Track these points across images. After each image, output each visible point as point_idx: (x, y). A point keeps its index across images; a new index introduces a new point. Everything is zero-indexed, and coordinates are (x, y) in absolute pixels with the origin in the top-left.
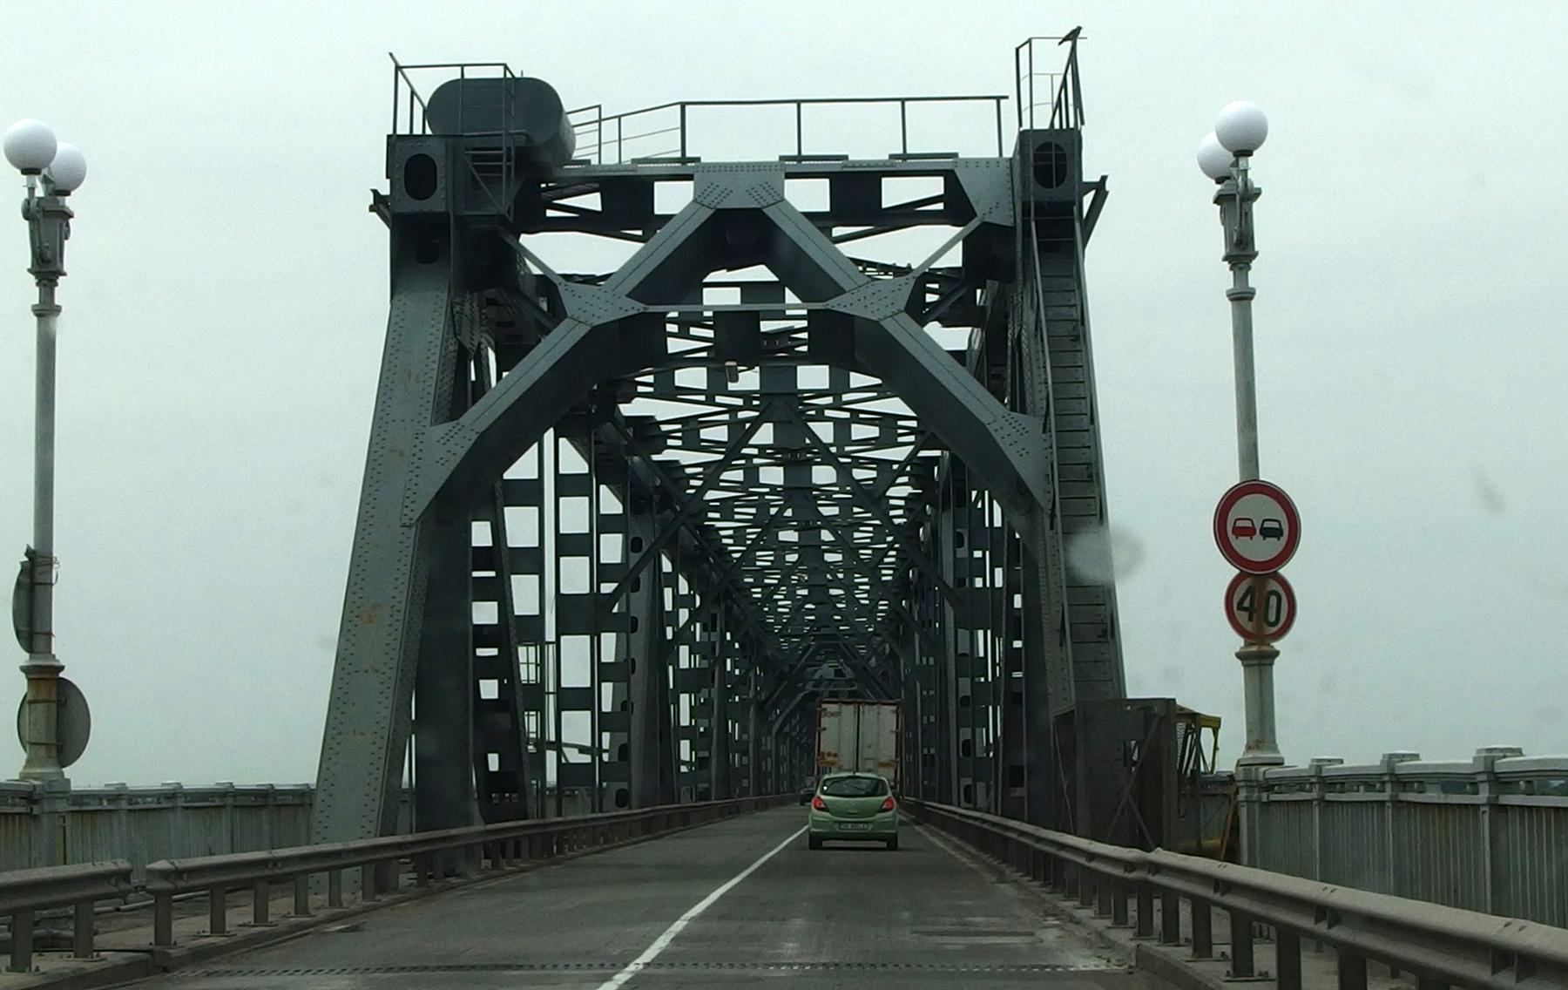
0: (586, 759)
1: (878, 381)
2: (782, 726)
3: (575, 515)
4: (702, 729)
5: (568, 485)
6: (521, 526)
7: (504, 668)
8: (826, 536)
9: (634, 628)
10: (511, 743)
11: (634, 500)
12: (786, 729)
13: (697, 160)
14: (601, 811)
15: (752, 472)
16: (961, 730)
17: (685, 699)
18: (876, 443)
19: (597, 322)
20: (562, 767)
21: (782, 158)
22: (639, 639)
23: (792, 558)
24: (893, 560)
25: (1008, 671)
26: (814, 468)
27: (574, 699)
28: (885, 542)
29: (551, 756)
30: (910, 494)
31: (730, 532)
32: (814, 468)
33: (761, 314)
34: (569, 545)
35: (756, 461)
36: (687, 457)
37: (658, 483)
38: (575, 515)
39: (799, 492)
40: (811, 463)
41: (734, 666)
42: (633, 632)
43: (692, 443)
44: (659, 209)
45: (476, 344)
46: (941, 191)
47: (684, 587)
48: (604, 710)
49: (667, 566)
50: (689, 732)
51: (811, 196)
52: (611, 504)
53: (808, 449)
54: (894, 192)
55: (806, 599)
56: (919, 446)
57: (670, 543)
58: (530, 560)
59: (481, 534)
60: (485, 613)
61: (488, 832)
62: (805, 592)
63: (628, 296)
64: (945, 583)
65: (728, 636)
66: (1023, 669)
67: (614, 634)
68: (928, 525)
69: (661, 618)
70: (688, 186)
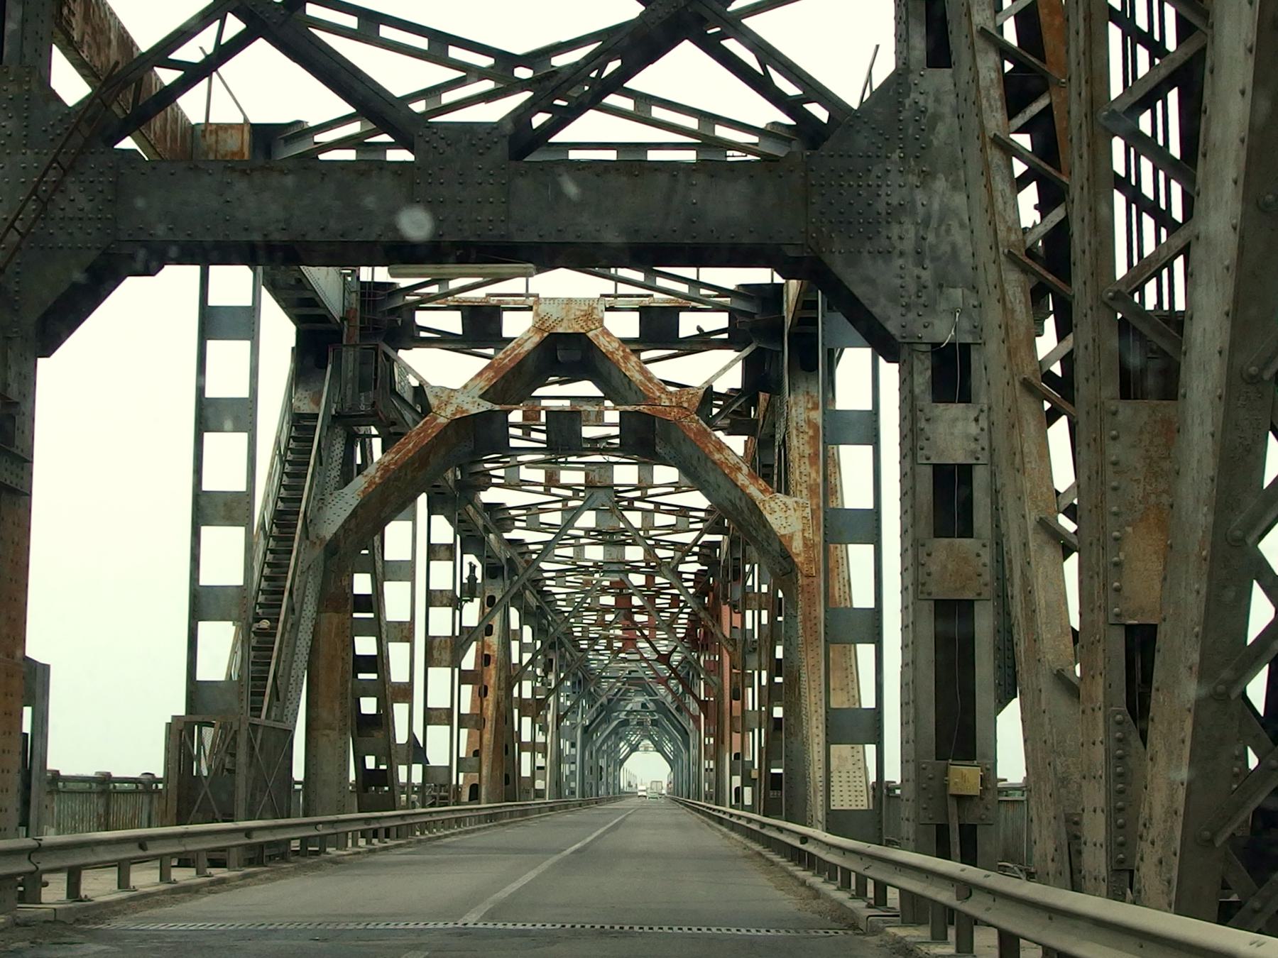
23: (609, 617)
44: (506, 333)
68: (711, 594)
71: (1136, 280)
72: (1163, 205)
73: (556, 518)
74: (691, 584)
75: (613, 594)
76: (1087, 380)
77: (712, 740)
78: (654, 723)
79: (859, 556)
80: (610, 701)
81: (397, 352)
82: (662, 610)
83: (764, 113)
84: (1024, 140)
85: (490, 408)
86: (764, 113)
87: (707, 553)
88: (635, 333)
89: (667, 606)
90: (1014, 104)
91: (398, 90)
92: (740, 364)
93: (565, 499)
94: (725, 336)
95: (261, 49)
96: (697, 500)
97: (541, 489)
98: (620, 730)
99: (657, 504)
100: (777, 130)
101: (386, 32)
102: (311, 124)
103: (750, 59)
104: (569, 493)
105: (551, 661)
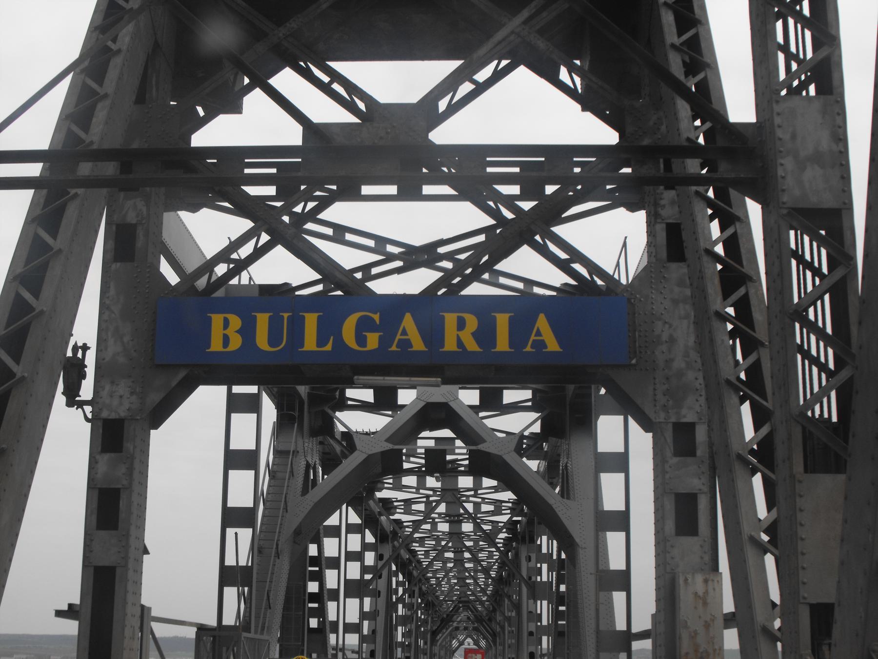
2: (442, 642)
3: (354, 542)
6: (331, 547)
7: (321, 613)
8: (467, 555)
11: (382, 537)
15: (434, 525)
16: (529, 647)
19: (370, 453)
22: (382, 601)
23: (450, 565)
27: (350, 628)
31: (423, 552)
34: (352, 556)
35: (436, 520)
37: (408, 557)
38: (354, 542)
39: (456, 535)
40: (464, 551)
43: (408, 511)
44: (400, 402)
47: (401, 578)
49: (394, 568)
50: (402, 644)
52: (370, 538)
53: (461, 515)
58: (334, 563)
59: (313, 550)
60: (313, 587)
66: (566, 619)
68: (513, 551)
69: (391, 591)
71: (809, 405)
72: (806, 347)
73: (421, 507)
74: (501, 545)
75: (453, 552)
76: (784, 462)
77: (513, 641)
78: (475, 629)
79: (614, 540)
80: (448, 615)
81: (335, 413)
82: (483, 561)
83: (558, 278)
84: (731, 311)
85: (391, 448)
86: (558, 278)
87: (511, 526)
88: (477, 403)
89: (486, 558)
90: (726, 295)
91: (348, 265)
92: (539, 422)
93: (428, 497)
94: (530, 404)
95: (279, 251)
96: (508, 496)
97: (414, 490)
98: (453, 633)
99: (483, 499)
100: (567, 289)
101: (349, 237)
102: (294, 285)
103: (553, 248)
104: (431, 493)
105: (414, 591)
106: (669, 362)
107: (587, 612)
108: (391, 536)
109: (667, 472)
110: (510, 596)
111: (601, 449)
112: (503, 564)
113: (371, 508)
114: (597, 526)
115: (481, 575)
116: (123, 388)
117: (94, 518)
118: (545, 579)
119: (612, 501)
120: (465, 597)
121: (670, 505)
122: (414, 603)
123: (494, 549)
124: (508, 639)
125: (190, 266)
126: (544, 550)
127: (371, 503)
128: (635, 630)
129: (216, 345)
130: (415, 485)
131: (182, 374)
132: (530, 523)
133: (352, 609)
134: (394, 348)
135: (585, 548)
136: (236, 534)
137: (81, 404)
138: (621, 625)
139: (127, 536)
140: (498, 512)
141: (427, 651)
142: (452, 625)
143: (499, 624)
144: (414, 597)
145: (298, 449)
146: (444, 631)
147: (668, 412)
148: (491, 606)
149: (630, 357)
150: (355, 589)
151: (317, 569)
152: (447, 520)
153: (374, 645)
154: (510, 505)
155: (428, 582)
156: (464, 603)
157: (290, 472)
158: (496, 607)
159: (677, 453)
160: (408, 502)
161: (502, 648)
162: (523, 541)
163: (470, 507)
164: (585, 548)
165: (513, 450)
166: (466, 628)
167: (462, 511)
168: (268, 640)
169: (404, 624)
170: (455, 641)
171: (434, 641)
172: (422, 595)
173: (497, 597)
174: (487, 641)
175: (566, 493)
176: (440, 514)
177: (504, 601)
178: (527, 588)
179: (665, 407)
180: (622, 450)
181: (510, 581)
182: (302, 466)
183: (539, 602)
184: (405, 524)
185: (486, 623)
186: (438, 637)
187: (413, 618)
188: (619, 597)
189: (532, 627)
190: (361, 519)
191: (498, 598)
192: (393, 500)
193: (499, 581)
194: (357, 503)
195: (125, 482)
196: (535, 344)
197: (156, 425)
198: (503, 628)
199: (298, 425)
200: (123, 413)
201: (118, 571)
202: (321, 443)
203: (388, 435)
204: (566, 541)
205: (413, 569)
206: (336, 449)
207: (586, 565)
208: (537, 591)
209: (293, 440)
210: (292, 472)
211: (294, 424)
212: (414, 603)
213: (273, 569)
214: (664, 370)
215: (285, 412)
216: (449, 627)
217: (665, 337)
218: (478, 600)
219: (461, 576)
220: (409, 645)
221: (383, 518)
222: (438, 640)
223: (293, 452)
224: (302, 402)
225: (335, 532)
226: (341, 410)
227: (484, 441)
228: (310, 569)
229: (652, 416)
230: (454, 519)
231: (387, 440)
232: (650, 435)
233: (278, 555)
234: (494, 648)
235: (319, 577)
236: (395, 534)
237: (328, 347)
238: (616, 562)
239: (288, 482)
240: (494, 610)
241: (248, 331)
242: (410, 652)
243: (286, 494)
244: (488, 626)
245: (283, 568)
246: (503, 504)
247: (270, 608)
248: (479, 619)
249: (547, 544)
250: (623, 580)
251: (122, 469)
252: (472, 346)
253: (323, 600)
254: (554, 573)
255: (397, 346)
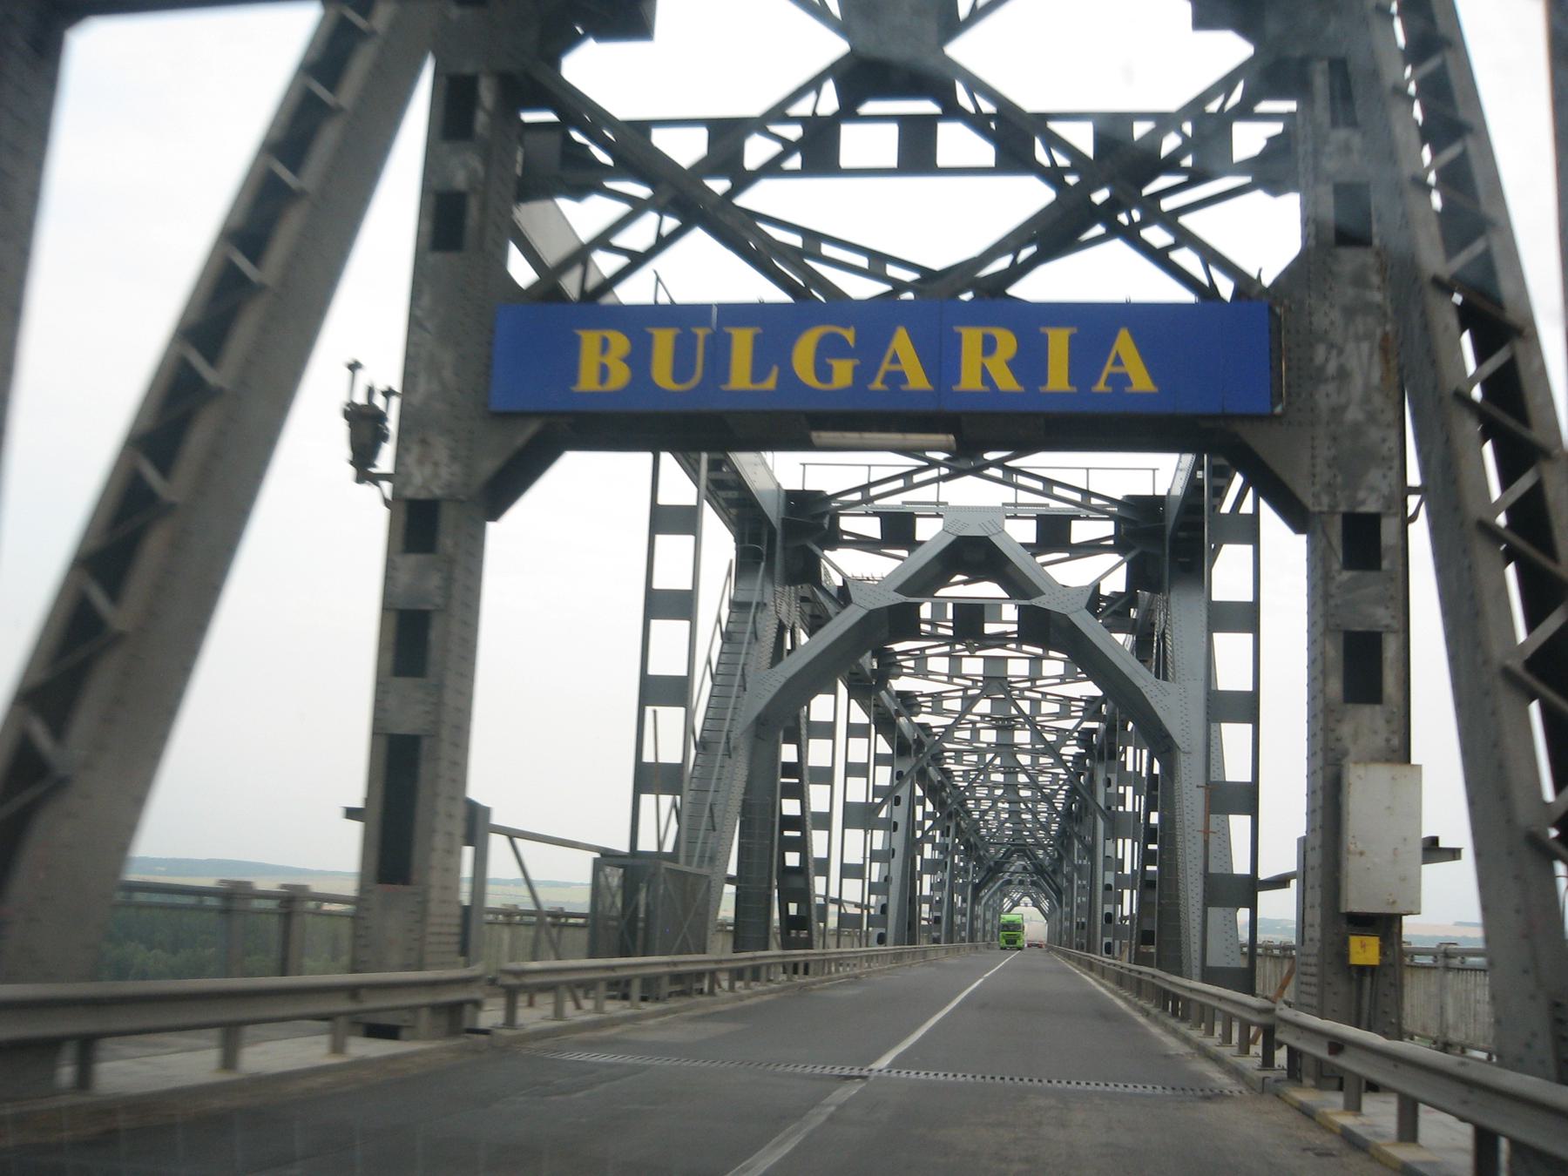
0: (858, 911)
1: (1066, 656)
2: (988, 900)
3: (859, 750)
4: (937, 899)
5: (854, 731)
6: (819, 753)
7: (802, 846)
8: (1022, 778)
9: (895, 828)
10: (804, 895)
11: (902, 747)
12: (991, 902)
13: (946, 503)
14: (867, 946)
15: (975, 732)
16: (1105, 906)
17: (927, 879)
18: (1058, 716)
19: (872, 607)
20: (842, 918)
21: (1004, 504)
22: (899, 839)
23: (999, 792)
24: (1063, 797)
25: (1143, 864)
26: (1016, 732)
27: (848, 871)
28: (1058, 784)
29: (833, 909)
30: (1077, 753)
31: (961, 773)
32: (1016, 732)
33: (987, 611)
34: (853, 770)
35: (978, 725)
36: (935, 721)
37: (939, 779)
38: (859, 750)
39: (1006, 748)
40: (1017, 773)
41: (961, 860)
42: (894, 831)
43: (938, 711)
44: (918, 538)
45: (791, 622)
46: (1112, 532)
47: (929, 807)
48: (873, 880)
49: (919, 792)
50: (929, 900)
51: (1024, 532)
52: (884, 747)
53: (1013, 718)
54: (1081, 532)
55: (1006, 820)
56: (1083, 720)
57: (922, 776)
58: (825, 776)
59: (788, 753)
60: (791, 807)
61: (784, 956)
62: (1007, 816)
63: (895, 591)
64: (1097, 804)
65: (957, 840)
66: (1158, 863)
67: (882, 832)
68: (1087, 774)
69: (912, 824)
70: (940, 521)
78: (1033, 883)
79: (1234, 736)
80: (996, 863)
85: (904, 601)
94: (1111, 542)
99: (1044, 694)
102: (829, 493)
104: (969, 683)
106: (1338, 411)
107: (1189, 848)
108: (914, 747)
109: (1332, 596)
110: (1081, 837)
111: (1215, 598)
112: (1070, 794)
113: (883, 703)
114: (1208, 713)
115: (1042, 807)
116: (441, 448)
117: (389, 657)
118: (1129, 808)
119: (1232, 675)
120: (1019, 839)
121: (1334, 652)
122: (947, 845)
123: (1061, 771)
124: (1078, 896)
125: (551, 256)
126: (1130, 768)
127: (883, 693)
128: (1263, 875)
129: (588, 381)
130: (947, 671)
131: (533, 427)
132: (1111, 730)
133: (854, 847)
134: (878, 385)
135: (1189, 753)
136: (655, 712)
137: (375, 479)
138: (1241, 866)
139: (440, 687)
140: (1064, 714)
141: (966, 911)
142: (1002, 877)
143: (1066, 876)
144: (948, 836)
145: (766, 601)
146: (991, 885)
147: (1335, 495)
148: (1056, 853)
149: (1271, 404)
150: (860, 816)
151: (797, 781)
152: (993, 724)
153: (885, 897)
154: (1083, 704)
155: (969, 817)
156: (1022, 850)
157: (751, 633)
158: (1064, 855)
159: (1349, 564)
160: (937, 698)
161: (1069, 909)
162: (1101, 758)
163: (1025, 706)
164: (1189, 753)
165: (1084, 605)
166: (1021, 882)
167: (1014, 711)
168: (707, 876)
169: (933, 873)
170: (1006, 899)
171: (976, 898)
172: (959, 832)
173: (1064, 840)
174: (1051, 902)
175: (1162, 672)
176: (983, 716)
177: (1073, 844)
178: (1103, 820)
179: (1330, 487)
180: (1250, 599)
181: (1081, 817)
182: (770, 631)
183: (1120, 841)
184: (935, 730)
185: (1048, 875)
186: (983, 893)
187: (946, 863)
188: (1239, 824)
189: (1110, 878)
190: (869, 717)
191: (1065, 842)
192: (917, 694)
193: (1067, 814)
194: (863, 689)
195: (439, 600)
196: (1112, 380)
197: (495, 512)
198: (1071, 881)
199: (766, 565)
200: (438, 492)
201: (425, 744)
202: (804, 599)
203: (899, 582)
204: (1160, 743)
205: (947, 797)
206: (829, 611)
207: (1190, 771)
208: (1117, 828)
209: (758, 589)
210: (755, 635)
211: (759, 564)
212: (947, 845)
213: (720, 773)
214: (1328, 423)
215: (747, 545)
216: (999, 879)
217: (1332, 368)
218: (1039, 845)
219: (1014, 807)
220: (940, 902)
221: (903, 720)
222: (983, 897)
223: (758, 604)
224: (772, 532)
225: (827, 730)
226: (833, 547)
227: (1040, 593)
228: (783, 780)
229: (1308, 501)
230: (1005, 726)
231: (899, 590)
232: (1303, 538)
233: (728, 753)
234: (1059, 910)
235: (799, 793)
236: (919, 743)
237: (770, 384)
238: (1236, 770)
239: (748, 648)
240: (1061, 858)
241: (639, 359)
242: (941, 911)
243: (744, 664)
244: (1052, 880)
245: (739, 771)
246: (1072, 703)
247: (714, 830)
248: (1039, 869)
249: (1134, 758)
250: (1247, 798)
251: (434, 581)
252: (1007, 382)
253: (805, 825)
254: (1143, 797)
255: (883, 382)
